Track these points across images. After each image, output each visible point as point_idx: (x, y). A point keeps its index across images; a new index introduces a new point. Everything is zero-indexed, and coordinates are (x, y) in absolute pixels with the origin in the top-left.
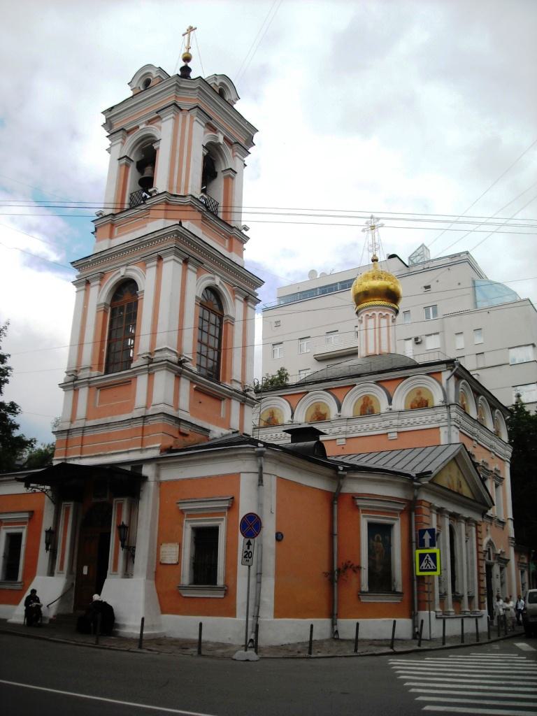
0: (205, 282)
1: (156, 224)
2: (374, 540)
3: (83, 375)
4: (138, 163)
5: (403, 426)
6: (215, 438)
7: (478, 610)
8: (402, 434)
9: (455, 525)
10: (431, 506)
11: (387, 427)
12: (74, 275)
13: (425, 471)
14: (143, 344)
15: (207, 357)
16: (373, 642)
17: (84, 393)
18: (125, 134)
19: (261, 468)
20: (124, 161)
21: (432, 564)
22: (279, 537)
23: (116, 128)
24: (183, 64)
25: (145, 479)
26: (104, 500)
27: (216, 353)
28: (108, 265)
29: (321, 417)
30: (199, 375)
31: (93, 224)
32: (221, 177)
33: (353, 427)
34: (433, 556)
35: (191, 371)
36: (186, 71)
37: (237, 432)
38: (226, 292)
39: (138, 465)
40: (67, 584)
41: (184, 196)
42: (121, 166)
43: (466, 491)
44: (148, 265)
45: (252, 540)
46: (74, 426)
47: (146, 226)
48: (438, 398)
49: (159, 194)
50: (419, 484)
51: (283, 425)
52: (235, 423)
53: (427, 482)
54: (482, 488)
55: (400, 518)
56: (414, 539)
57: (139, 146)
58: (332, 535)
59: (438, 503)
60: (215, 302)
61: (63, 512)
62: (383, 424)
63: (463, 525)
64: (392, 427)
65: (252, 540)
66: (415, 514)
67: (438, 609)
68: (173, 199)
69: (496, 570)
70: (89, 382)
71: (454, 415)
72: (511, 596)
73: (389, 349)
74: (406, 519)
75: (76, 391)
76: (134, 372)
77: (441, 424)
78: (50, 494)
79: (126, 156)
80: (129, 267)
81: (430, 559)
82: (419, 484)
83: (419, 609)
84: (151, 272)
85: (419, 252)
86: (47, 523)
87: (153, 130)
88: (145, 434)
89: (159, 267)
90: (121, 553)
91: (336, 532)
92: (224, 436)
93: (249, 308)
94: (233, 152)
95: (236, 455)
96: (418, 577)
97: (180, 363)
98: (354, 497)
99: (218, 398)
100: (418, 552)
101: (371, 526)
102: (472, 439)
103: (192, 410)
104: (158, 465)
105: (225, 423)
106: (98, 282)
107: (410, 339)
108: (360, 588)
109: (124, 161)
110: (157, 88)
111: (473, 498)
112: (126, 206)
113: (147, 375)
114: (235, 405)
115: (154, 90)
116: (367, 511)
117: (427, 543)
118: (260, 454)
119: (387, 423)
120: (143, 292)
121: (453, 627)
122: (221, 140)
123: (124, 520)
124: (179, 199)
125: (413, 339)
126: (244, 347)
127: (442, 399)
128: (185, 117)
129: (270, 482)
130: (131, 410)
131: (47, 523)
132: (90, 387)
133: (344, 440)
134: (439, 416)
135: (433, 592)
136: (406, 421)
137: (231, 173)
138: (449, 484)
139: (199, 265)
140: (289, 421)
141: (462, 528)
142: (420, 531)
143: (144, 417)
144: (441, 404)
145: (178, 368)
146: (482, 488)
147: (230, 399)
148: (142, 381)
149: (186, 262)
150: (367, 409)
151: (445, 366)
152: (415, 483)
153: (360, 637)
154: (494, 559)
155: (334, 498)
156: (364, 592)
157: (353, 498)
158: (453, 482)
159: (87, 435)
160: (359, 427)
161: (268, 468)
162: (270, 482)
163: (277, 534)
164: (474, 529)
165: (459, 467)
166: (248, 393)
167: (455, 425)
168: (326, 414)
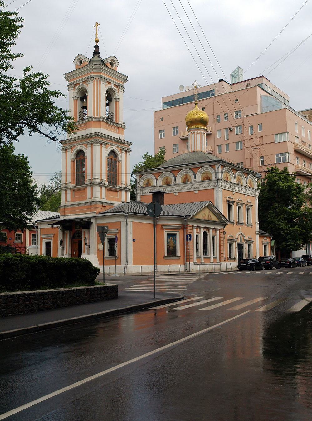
0: (110, 149)
5: (200, 188)
6: (116, 206)
8: (200, 191)
9: (207, 231)
10: (193, 227)
11: (194, 188)
18: (74, 85)
19: (127, 220)
22: (134, 240)
24: (95, 44)
25: (92, 223)
26: (79, 230)
33: (181, 188)
36: (96, 53)
38: (118, 151)
39: (89, 219)
47: (86, 129)
51: (153, 186)
52: (123, 199)
57: (94, 334)
59: (196, 225)
69: (245, 246)
73: (201, 149)
76: (86, 186)
77: (215, 187)
78: (60, 228)
80: (81, 146)
84: (89, 149)
85: (236, 71)
86: (60, 238)
88: (91, 208)
89: (92, 147)
90: (86, 247)
97: (101, 183)
99: (116, 191)
101: (168, 234)
104: (96, 219)
105: (119, 200)
106: (70, 150)
111: (219, 221)
113: (90, 187)
118: (126, 216)
119: (194, 186)
122: (113, 86)
125: (229, 129)
132: (71, 190)
134: (214, 184)
136: (201, 186)
139: (106, 144)
141: (211, 234)
142: (187, 235)
143: (90, 202)
147: (121, 191)
148: (89, 189)
149: (101, 144)
150: (186, 180)
151: (216, 162)
159: (71, 207)
161: (128, 220)
163: (133, 240)
164: (218, 232)
168: (170, 182)
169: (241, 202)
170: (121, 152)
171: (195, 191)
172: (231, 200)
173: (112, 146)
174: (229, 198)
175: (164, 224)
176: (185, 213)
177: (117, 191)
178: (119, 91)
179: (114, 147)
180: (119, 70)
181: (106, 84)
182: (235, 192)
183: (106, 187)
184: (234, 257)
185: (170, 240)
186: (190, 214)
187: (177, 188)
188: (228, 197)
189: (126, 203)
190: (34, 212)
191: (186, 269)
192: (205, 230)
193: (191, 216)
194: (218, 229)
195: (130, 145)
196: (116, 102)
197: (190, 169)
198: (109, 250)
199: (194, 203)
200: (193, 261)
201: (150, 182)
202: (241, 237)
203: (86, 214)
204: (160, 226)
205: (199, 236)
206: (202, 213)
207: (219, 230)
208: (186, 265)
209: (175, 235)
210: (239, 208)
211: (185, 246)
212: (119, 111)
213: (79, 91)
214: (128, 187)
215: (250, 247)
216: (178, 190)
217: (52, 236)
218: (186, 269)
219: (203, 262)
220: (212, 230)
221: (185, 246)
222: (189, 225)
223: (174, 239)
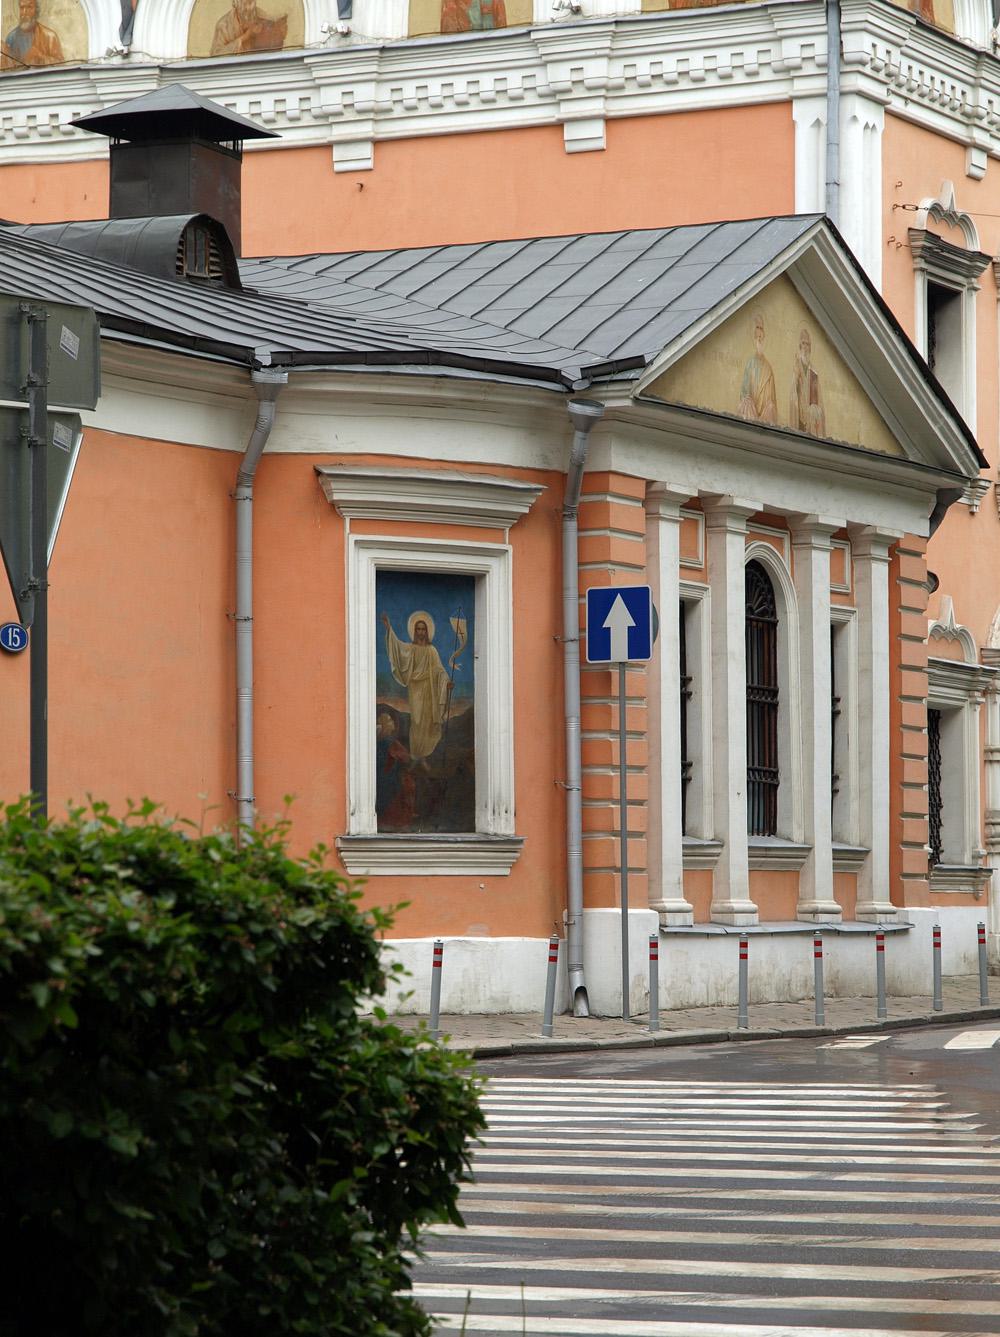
7: (889, 907)
8: (628, 126)
9: (780, 562)
10: (652, 496)
11: (556, 96)
13: (617, 357)
33: (409, 91)
50: (589, 411)
51: (83, 70)
53: (628, 403)
55: (510, 548)
56: (572, 628)
58: (231, 618)
59: (684, 479)
63: (820, 562)
64: (579, 92)
66: (580, 530)
67: (674, 900)
74: (542, 546)
77: (801, 86)
82: (589, 411)
83: (587, 902)
91: (246, 610)
98: (319, 474)
101: (389, 581)
102: (965, 146)
108: (344, 824)
116: (374, 518)
119: (561, 75)
133: (367, 150)
134: (791, 50)
135: (651, 833)
136: (644, 68)
138: (749, 393)
140: (110, 53)
152: (576, 408)
157: (318, 473)
160: (435, 88)
164: (880, 572)
167: (860, 94)
168: (284, 19)
171: (570, 132)
172: (950, 236)
174: (935, 210)
175: (339, 458)
176: (567, 336)
184: (976, 857)
185: (407, 651)
187: (365, 94)
188: (928, 203)
191: (582, 991)
192: (762, 550)
194: (879, 540)
199: (731, 235)
200: (651, 900)
201: (53, 23)
204: (302, 481)
206: (738, 348)
207: (895, 549)
208: (582, 947)
209: (463, 587)
211: (573, 727)
216: (379, 114)
218: (582, 991)
219: (682, 903)
220: (826, 543)
221: (573, 727)
222: (615, 484)
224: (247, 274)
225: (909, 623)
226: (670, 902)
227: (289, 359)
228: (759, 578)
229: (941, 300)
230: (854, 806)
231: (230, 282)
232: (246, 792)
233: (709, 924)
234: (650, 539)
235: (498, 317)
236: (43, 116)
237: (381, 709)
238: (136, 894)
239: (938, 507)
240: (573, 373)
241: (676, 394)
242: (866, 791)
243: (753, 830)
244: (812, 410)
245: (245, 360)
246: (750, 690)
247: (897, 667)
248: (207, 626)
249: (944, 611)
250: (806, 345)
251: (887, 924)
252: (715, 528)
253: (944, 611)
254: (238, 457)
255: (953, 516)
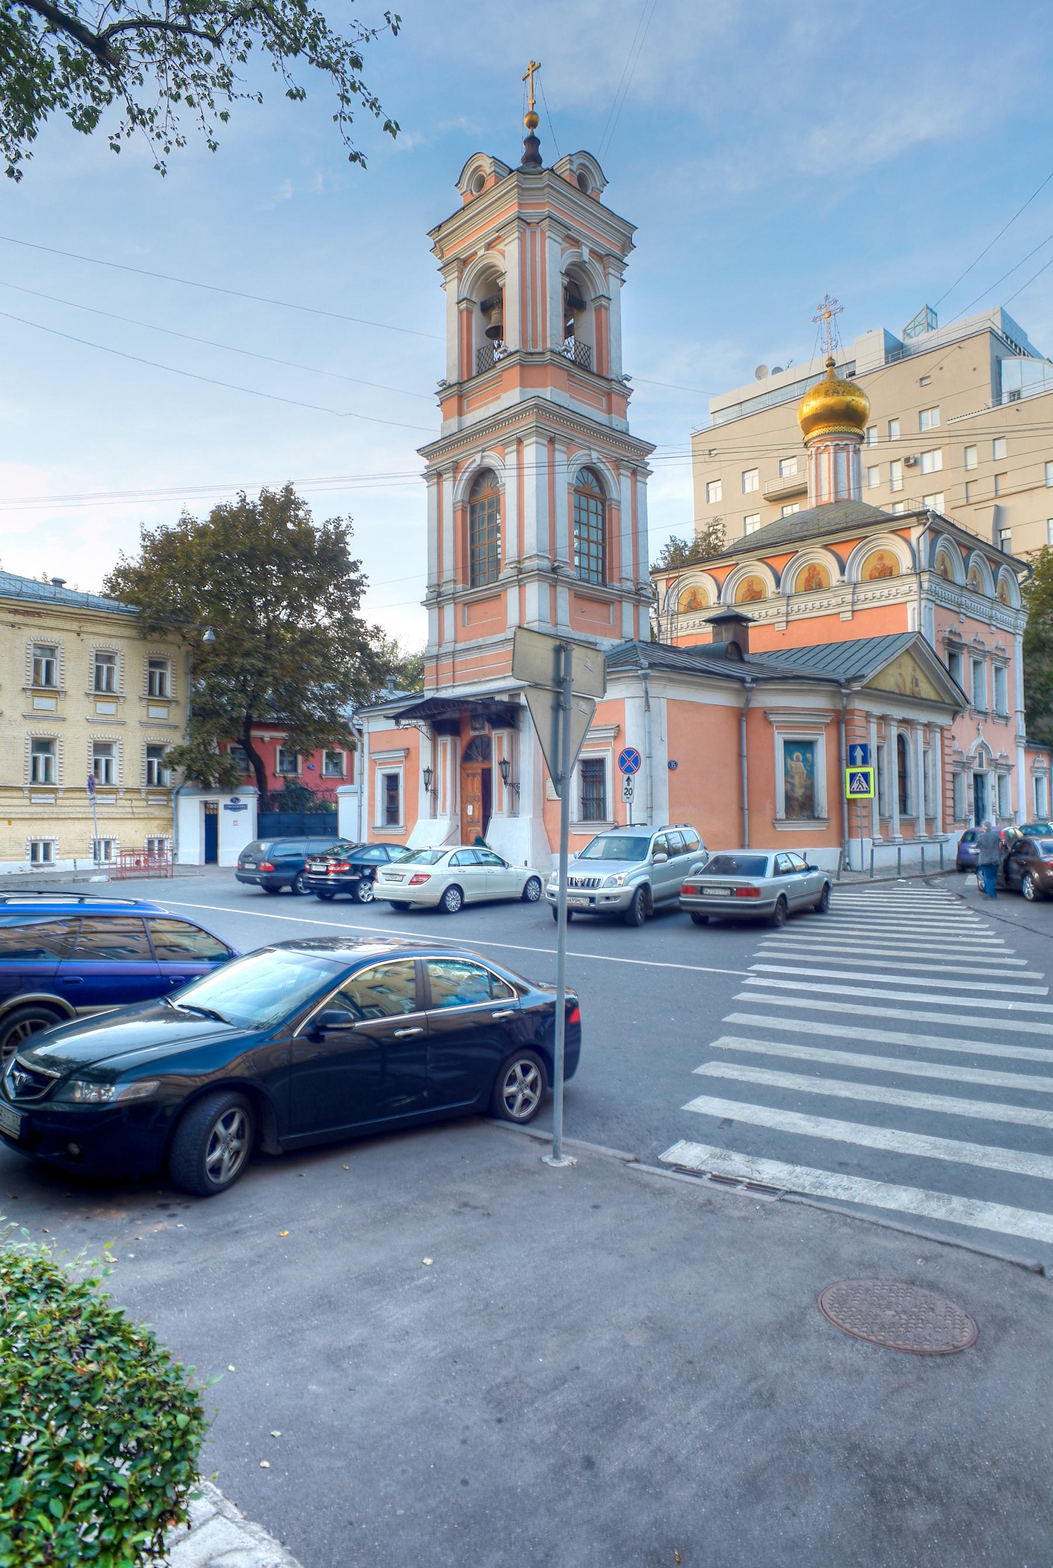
1: (511, 397)
2: (792, 759)
3: (448, 589)
4: (482, 304)
9: (908, 734)
10: (868, 715)
12: (422, 463)
14: (509, 549)
15: (588, 555)
16: (881, 870)
17: (449, 610)
19: (647, 692)
20: (464, 305)
21: (864, 784)
22: (672, 766)
23: (449, 255)
24: (527, 132)
26: (482, 732)
27: (600, 547)
28: (460, 451)
29: (755, 596)
30: (580, 580)
31: (437, 397)
32: (591, 307)
34: (866, 776)
35: (568, 577)
37: (631, 640)
39: (514, 692)
40: (451, 826)
41: (542, 353)
42: (460, 312)
43: (926, 690)
44: (507, 451)
45: (631, 776)
46: (443, 651)
47: (499, 398)
48: (905, 562)
49: (511, 354)
52: (628, 630)
54: (950, 685)
56: (844, 756)
58: (740, 756)
59: (877, 709)
60: (595, 483)
61: (440, 748)
62: (834, 601)
63: (920, 733)
65: (631, 776)
68: (530, 358)
69: (991, 780)
70: (454, 598)
71: (926, 585)
72: (1016, 812)
75: (441, 609)
79: (465, 299)
81: (862, 779)
87: (494, 258)
89: (519, 452)
92: (614, 647)
93: (638, 484)
94: (605, 268)
95: (619, 678)
96: (849, 800)
97: (554, 570)
98: (766, 713)
100: (849, 771)
101: (787, 743)
102: (958, 613)
103: (574, 623)
107: (899, 460)
109: (464, 305)
110: (494, 193)
112: (474, 374)
114: (628, 608)
115: (488, 197)
116: (784, 726)
117: (859, 761)
120: (504, 485)
121: (886, 857)
122: (586, 256)
123: (506, 756)
124: (536, 358)
126: (635, 533)
127: (910, 564)
128: (533, 234)
129: (659, 706)
130: (503, 630)
131: (425, 761)
137: (604, 302)
138: (898, 686)
141: (917, 740)
144: (909, 571)
145: (552, 575)
146: (950, 685)
147: (621, 602)
148: (512, 594)
149: (552, 441)
151: (914, 519)
152: (844, 691)
153: (902, 862)
154: (989, 765)
155: (742, 715)
156: (780, 820)
158: (904, 681)
159: (458, 660)
161: (655, 689)
162: (659, 706)
164: (938, 736)
165: (914, 660)
166: (643, 592)
169: (979, 647)
170: (619, 475)
172: (955, 639)
173: (587, 452)
174: (951, 632)
176: (841, 670)
177: (607, 603)
178: (606, 275)
179: (595, 455)
180: (603, 199)
181: (565, 245)
182: (967, 616)
183: (571, 586)
186: (859, 674)
189: (638, 644)
190: (123, 597)
192: (902, 731)
193: (866, 681)
194: (937, 726)
195: (650, 452)
196: (598, 310)
197: (826, 547)
198: (585, 802)
201: (699, 597)
202: (981, 755)
203: (504, 678)
205: (885, 747)
207: (942, 729)
209: (808, 746)
210: (976, 664)
212: (608, 341)
213: (477, 280)
214: (642, 589)
215: (1003, 783)
217: (402, 754)
219: (900, 835)
222: (856, 713)
223: (805, 760)
224: (746, 657)
225: (947, 751)
226: (876, 836)
227: (755, 680)
228: (901, 739)
229: (952, 657)
230: (931, 805)
231: (742, 660)
232: (746, 807)
233: (889, 841)
234: (867, 729)
235: (821, 665)
236: (691, 622)
237: (786, 782)
238: (855, 844)
239: (955, 714)
240: (843, 681)
241: (875, 685)
242: (935, 800)
243: (901, 813)
244: (916, 689)
245: (742, 680)
246: (899, 772)
247: (943, 763)
248: (732, 759)
249: (957, 745)
250: (914, 670)
251: (941, 839)
252: (888, 725)
253: (957, 745)
254: (739, 709)
255: (958, 719)
